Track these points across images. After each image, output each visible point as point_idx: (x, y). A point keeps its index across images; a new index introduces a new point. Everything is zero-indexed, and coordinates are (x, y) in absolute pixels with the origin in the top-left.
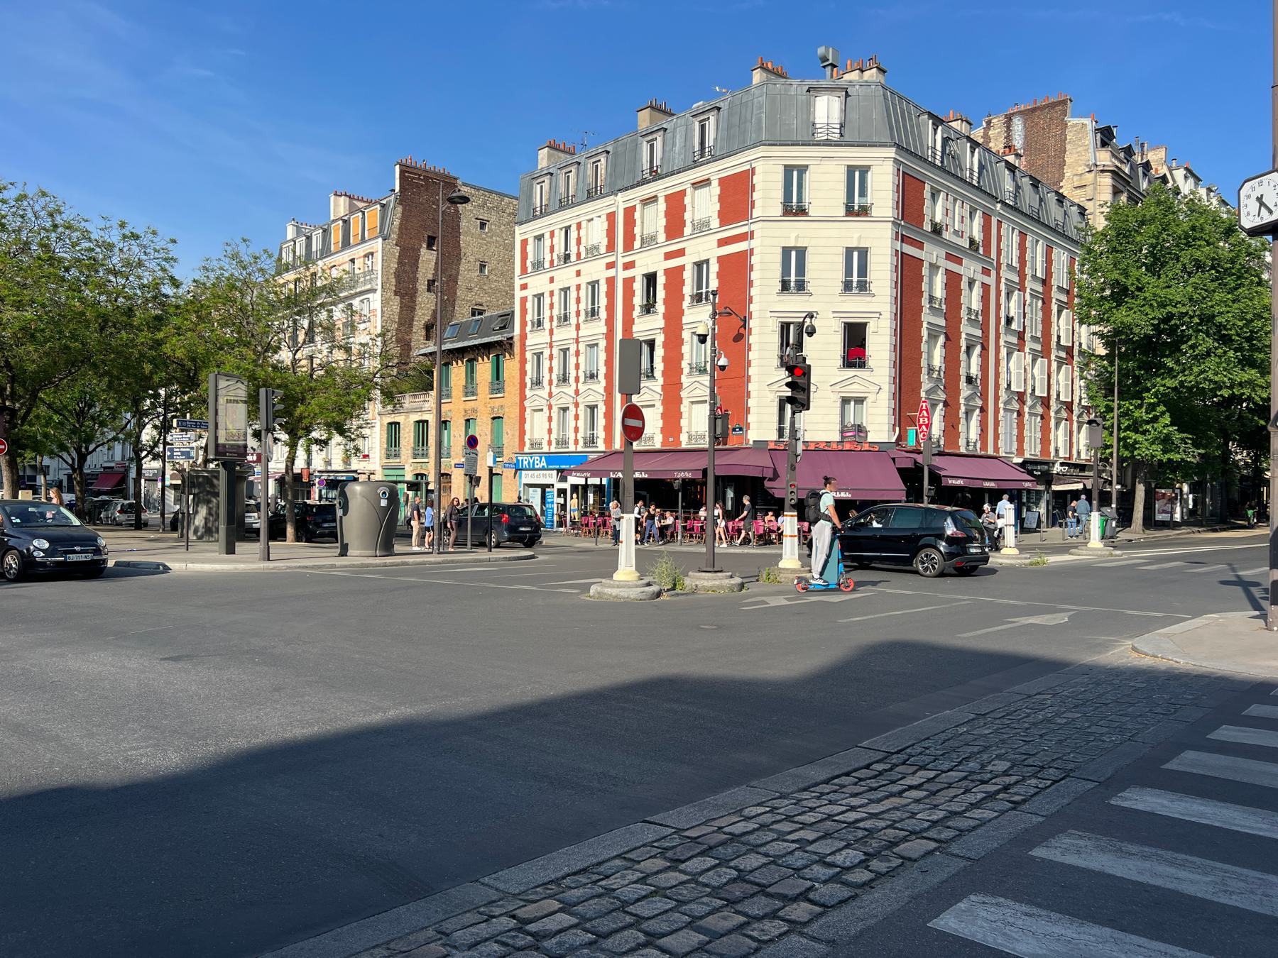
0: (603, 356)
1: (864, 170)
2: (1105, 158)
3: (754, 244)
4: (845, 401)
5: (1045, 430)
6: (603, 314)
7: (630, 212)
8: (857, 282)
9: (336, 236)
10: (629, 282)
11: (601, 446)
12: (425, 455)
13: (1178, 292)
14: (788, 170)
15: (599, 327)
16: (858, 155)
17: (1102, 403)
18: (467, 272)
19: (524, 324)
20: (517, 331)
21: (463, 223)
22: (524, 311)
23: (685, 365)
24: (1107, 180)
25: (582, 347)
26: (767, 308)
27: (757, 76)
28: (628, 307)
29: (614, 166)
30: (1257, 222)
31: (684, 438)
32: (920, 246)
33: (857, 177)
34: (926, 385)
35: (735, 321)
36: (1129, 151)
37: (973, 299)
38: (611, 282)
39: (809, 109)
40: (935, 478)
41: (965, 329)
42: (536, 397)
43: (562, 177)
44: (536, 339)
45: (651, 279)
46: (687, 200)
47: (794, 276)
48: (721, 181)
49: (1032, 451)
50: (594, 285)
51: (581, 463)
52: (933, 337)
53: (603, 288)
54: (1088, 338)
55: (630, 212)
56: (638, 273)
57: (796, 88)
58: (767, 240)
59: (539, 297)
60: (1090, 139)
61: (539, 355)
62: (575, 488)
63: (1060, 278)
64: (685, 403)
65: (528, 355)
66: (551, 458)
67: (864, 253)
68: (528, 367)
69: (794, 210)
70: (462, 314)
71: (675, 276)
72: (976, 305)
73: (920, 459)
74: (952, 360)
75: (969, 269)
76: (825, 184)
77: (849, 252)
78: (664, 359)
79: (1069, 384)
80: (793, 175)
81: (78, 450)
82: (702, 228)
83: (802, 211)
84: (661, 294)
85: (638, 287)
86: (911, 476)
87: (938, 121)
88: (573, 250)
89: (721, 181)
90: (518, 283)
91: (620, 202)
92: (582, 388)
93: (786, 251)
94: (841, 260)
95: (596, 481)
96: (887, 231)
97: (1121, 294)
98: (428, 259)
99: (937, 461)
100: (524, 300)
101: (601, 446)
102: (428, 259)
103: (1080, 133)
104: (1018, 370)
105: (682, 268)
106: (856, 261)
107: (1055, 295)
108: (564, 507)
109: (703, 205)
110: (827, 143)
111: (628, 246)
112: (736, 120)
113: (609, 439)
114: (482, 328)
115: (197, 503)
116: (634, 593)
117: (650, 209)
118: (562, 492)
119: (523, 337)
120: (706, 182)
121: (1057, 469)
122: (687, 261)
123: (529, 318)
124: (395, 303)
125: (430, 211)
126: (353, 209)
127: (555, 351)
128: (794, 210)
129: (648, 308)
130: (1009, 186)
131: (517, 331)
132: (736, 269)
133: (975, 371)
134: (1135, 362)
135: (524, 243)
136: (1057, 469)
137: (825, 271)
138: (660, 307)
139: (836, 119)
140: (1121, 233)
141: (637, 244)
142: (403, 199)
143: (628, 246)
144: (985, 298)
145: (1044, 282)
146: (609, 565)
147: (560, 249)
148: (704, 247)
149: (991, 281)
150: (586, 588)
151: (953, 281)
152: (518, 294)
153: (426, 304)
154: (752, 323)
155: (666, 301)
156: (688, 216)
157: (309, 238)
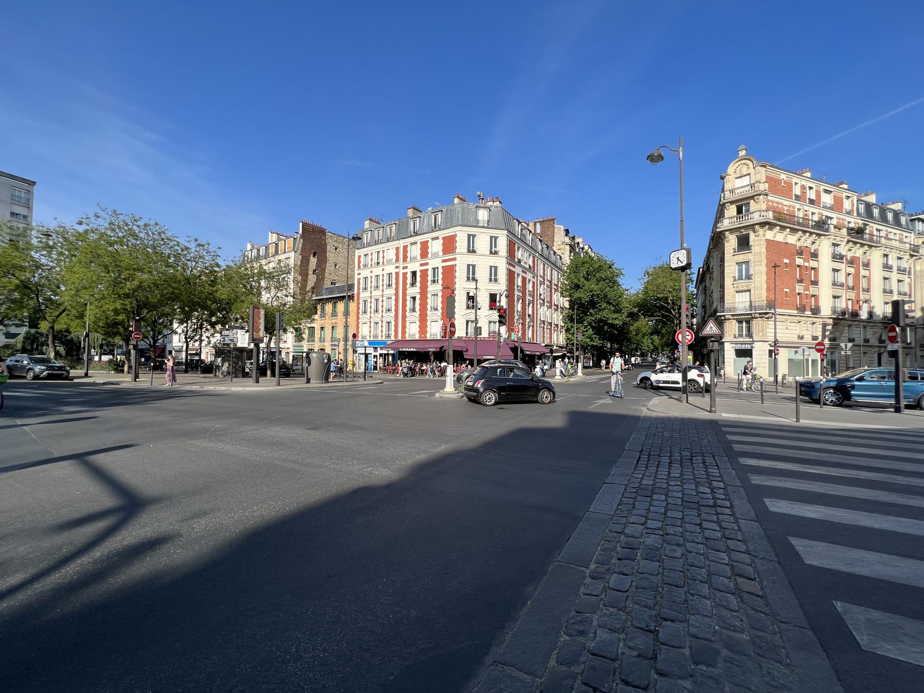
0: (394, 303)
1: (496, 238)
2: (567, 240)
3: (456, 262)
4: (490, 322)
5: (551, 334)
6: (394, 286)
7: (405, 247)
8: (493, 278)
9: (272, 250)
10: (405, 275)
11: (393, 338)
12: (313, 341)
13: (594, 287)
14: (469, 236)
15: (392, 291)
16: (495, 232)
17: (570, 325)
18: (329, 267)
19: (359, 289)
20: (356, 291)
21: (328, 248)
22: (359, 284)
23: (428, 307)
24: (568, 248)
25: (385, 299)
26: (462, 287)
27: (456, 200)
28: (405, 284)
29: (399, 229)
30: (677, 266)
31: (407, 335)
32: (514, 267)
33: (493, 240)
34: (516, 317)
35: (449, 291)
36: (573, 238)
37: (529, 287)
38: (397, 274)
39: (476, 214)
40: (522, 351)
41: (528, 297)
42: (363, 318)
43: (376, 233)
44: (364, 295)
45: (414, 274)
46: (429, 244)
47: (471, 276)
48: (443, 238)
49: (547, 342)
50: (390, 275)
51: (383, 344)
52: (518, 300)
53: (394, 276)
54: (565, 302)
55: (405, 247)
56: (409, 271)
57: (472, 206)
58: (461, 261)
59: (366, 278)
60: (563, 233)
61: (365, 301)
62: (381, 355)
63: (555, 281)
64: (429, 322)
65: (361, 301)
66: (370, 343)
67: (496, 268)
68: (361, 306)
69: (471, 251)
70: (327, 284)
71: (424, 273)
72: (531, 289)
73: (517, 344)
74: (524, 308)
75: (529, 276)
76: (482, 242)
77: (491, 267)
78: (420, 304)
79: (558, 318)
80: (471, 238)
81: (153, 338)
82: (435, 255)
83: (474, 251)
84: (418, 279)
85: (409, 276)
86: (514, 350)
87: (519, 223)
88: (381, 261)
89: (443, 238)
90: (356, 272)
91: (401, 243)
92: (384, 315)
93: (468, 266)
94: (488, 270)
95: (392, 352)
96: (504, 261)
97: (577, 287)
98: (313, 261)
99: (522, 345)
100: (359, 279)
101: (393, 338)
102: (313, 261)
103: (559, 230)
104: (544, 313)
105: (427, 270)
106: (494, 270)
107: (554, 287)
108: (376, 362)
109: (436, 247)
110: (483, 227)
111: (405, 260)
112: (449, 216)
113: (396, 335)
114: (340, 289)
115: (223, 361)
116: (455, 396)
117: (414, 247)
118: (375, 356)
119: (359, 294)
120: (437, 238)
121: (555, 348)
122: (430, 267)
123: (361, 286)
124: (299, 278)
125: (314, 241)
126: (279, 239)
127: (373, 300)
128: (471, 251)
129: (413, 284)
130: (540, 247)
131: (356, 291)
132: (449, 272)
133: (530, 312)
134: (580, 310)
135: (359, 257)
136: (555, 348)
137: (482, 274)
138: (418, 284)
139: (486, 219)
140: (575, 267)
141: (408, 260)
142: (303, 236)
143: (405, 260)
144: (533, 287)
145: (550, 282)
146: (443, 385)
147: (375, 260)
148: (436, 263)
149: (535, 280)
150: (434, 394)
151: (524, 279)
152: (356, 277)
153: (312, 279)
154: (456, 292)
155: (421, 282)
156: (429, 250)
157: (258, 250)
